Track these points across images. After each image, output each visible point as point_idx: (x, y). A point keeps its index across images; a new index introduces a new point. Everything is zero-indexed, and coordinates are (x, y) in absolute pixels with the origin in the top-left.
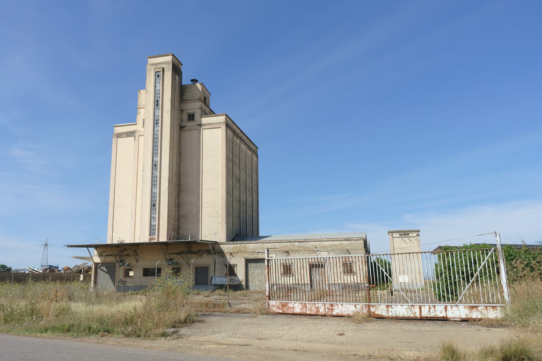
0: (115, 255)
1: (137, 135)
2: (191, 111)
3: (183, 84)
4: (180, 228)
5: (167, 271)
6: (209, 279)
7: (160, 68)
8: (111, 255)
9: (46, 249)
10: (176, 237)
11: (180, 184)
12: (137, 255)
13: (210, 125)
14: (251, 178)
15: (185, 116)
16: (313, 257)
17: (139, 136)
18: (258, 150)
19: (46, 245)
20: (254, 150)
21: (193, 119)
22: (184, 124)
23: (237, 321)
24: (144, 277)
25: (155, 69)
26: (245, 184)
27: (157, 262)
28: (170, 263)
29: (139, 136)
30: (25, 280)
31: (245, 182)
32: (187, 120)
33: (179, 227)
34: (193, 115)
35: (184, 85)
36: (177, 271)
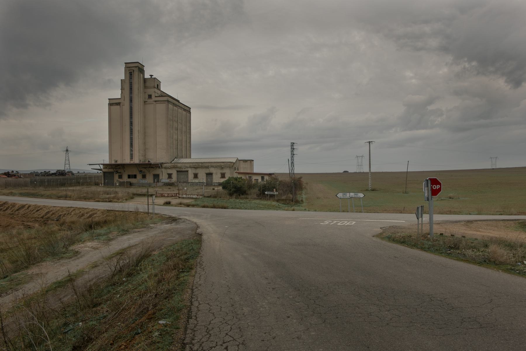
0: (113, 168)
1: (121, 105)
2: (150, 93)
3: (145, 78)
4: (146, 155)
5: (139, 176)
6: (160, 180)
7: (132, 70)
8: (111, 168)
9: (67, 154)
10: (169, 136)
11: (145, 132)
12: (124, 168)
13: (160, 102)
14: (186, 126)
15: (147, 97)
16: (208, 171)
17: (122, 105)
18: (191, 109)
19: (67, 151)
20: (188, 110)
21: (151, 98)
22: (146, 100)
23: (306, 208)
24: (129, 179)
25: (129, 70)
26: (181, 130)
27: (134, 171)
28: (141, 172)
29: (122, 105)
30: (200, 235)
31: (181, 129)
32: (148, 98)
33: (145, 154)
34: (151, 95)
35: (146, 78)
36: (144, 177)
